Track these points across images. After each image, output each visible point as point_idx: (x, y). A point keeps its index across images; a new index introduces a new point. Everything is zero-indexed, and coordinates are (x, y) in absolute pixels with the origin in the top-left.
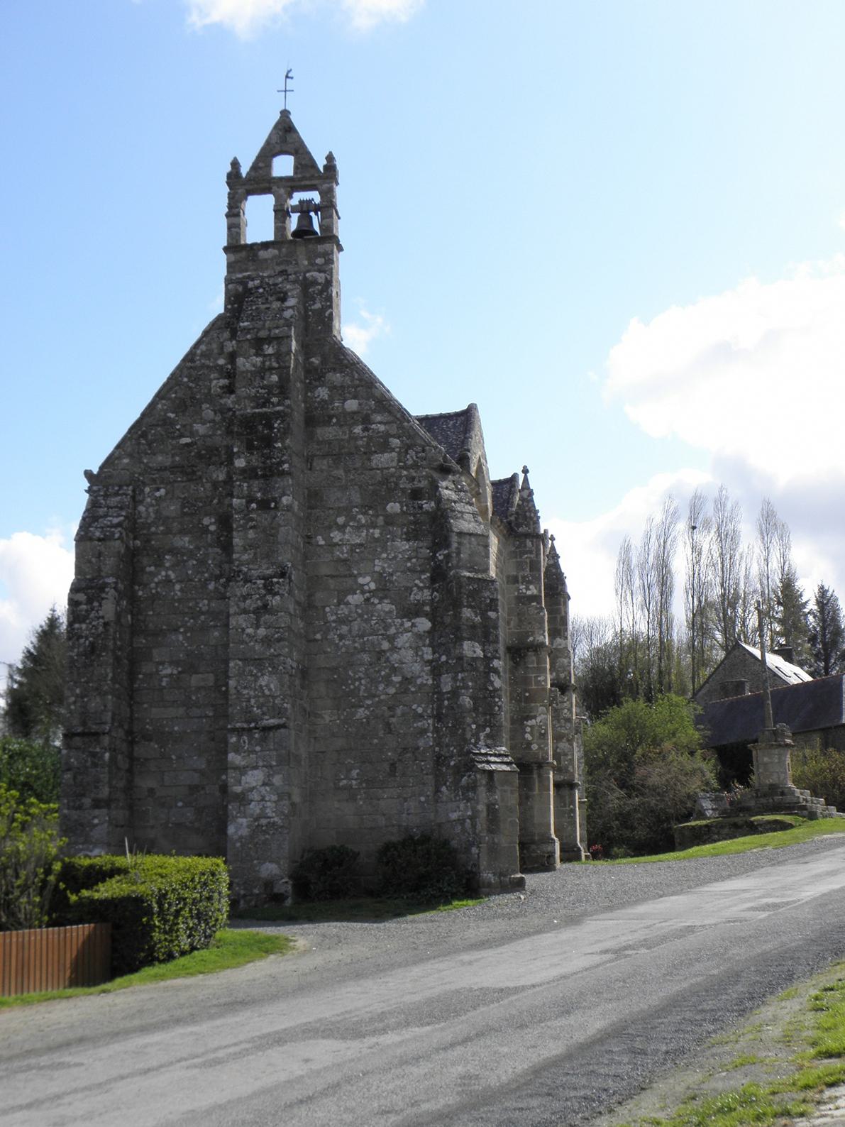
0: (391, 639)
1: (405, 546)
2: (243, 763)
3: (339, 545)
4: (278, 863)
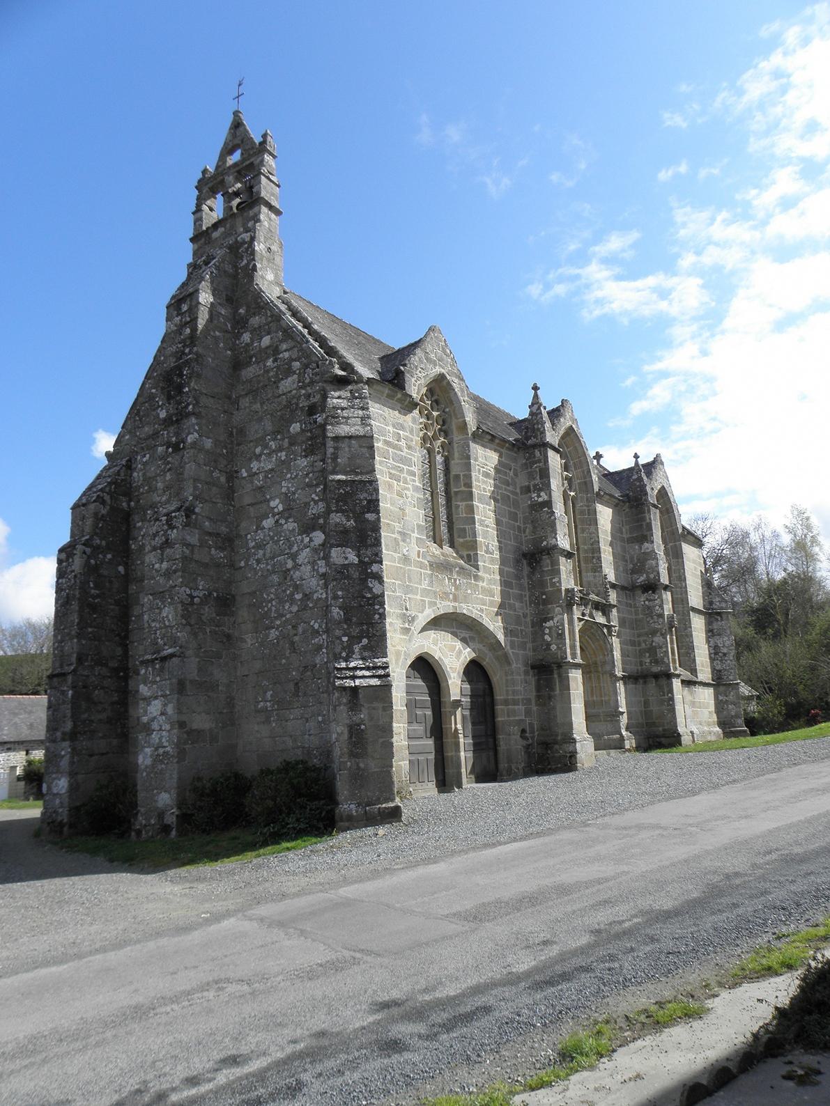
0: (294, 557)
2: (149, 694)
3: (257, 474)
4: (170, 793)
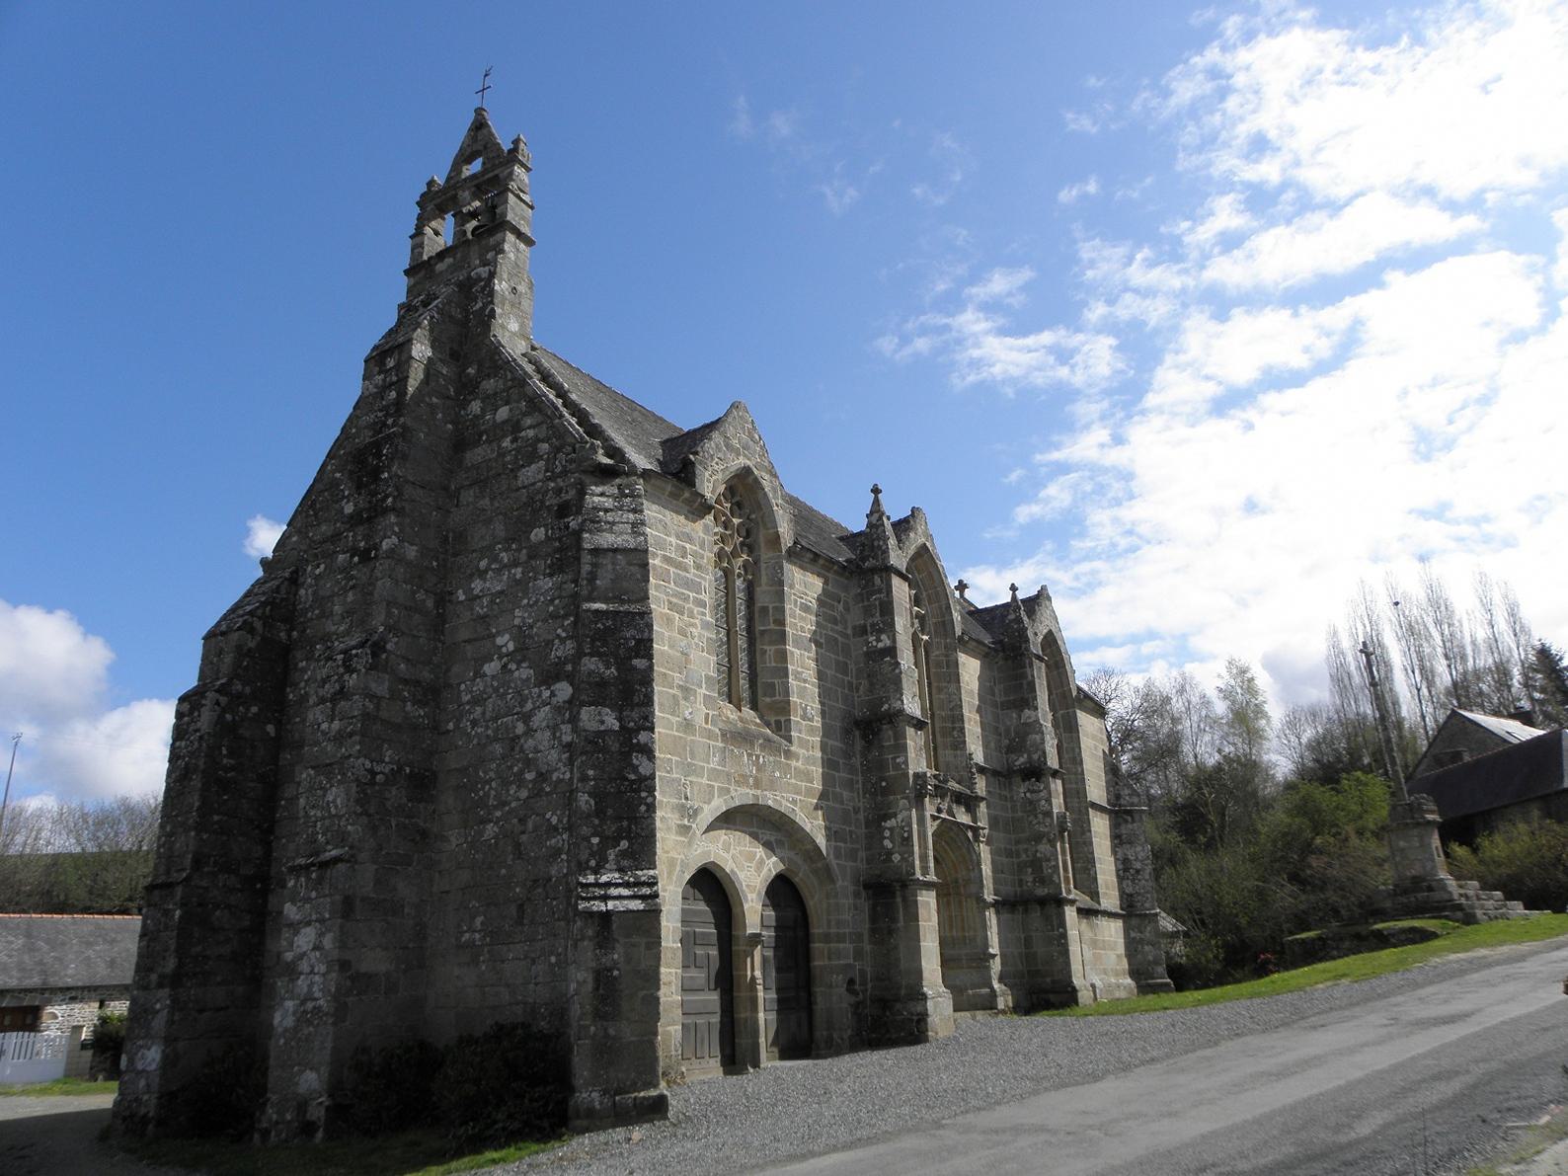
0: (526, 718)
1: (547, 583)
2: (297, 917)
